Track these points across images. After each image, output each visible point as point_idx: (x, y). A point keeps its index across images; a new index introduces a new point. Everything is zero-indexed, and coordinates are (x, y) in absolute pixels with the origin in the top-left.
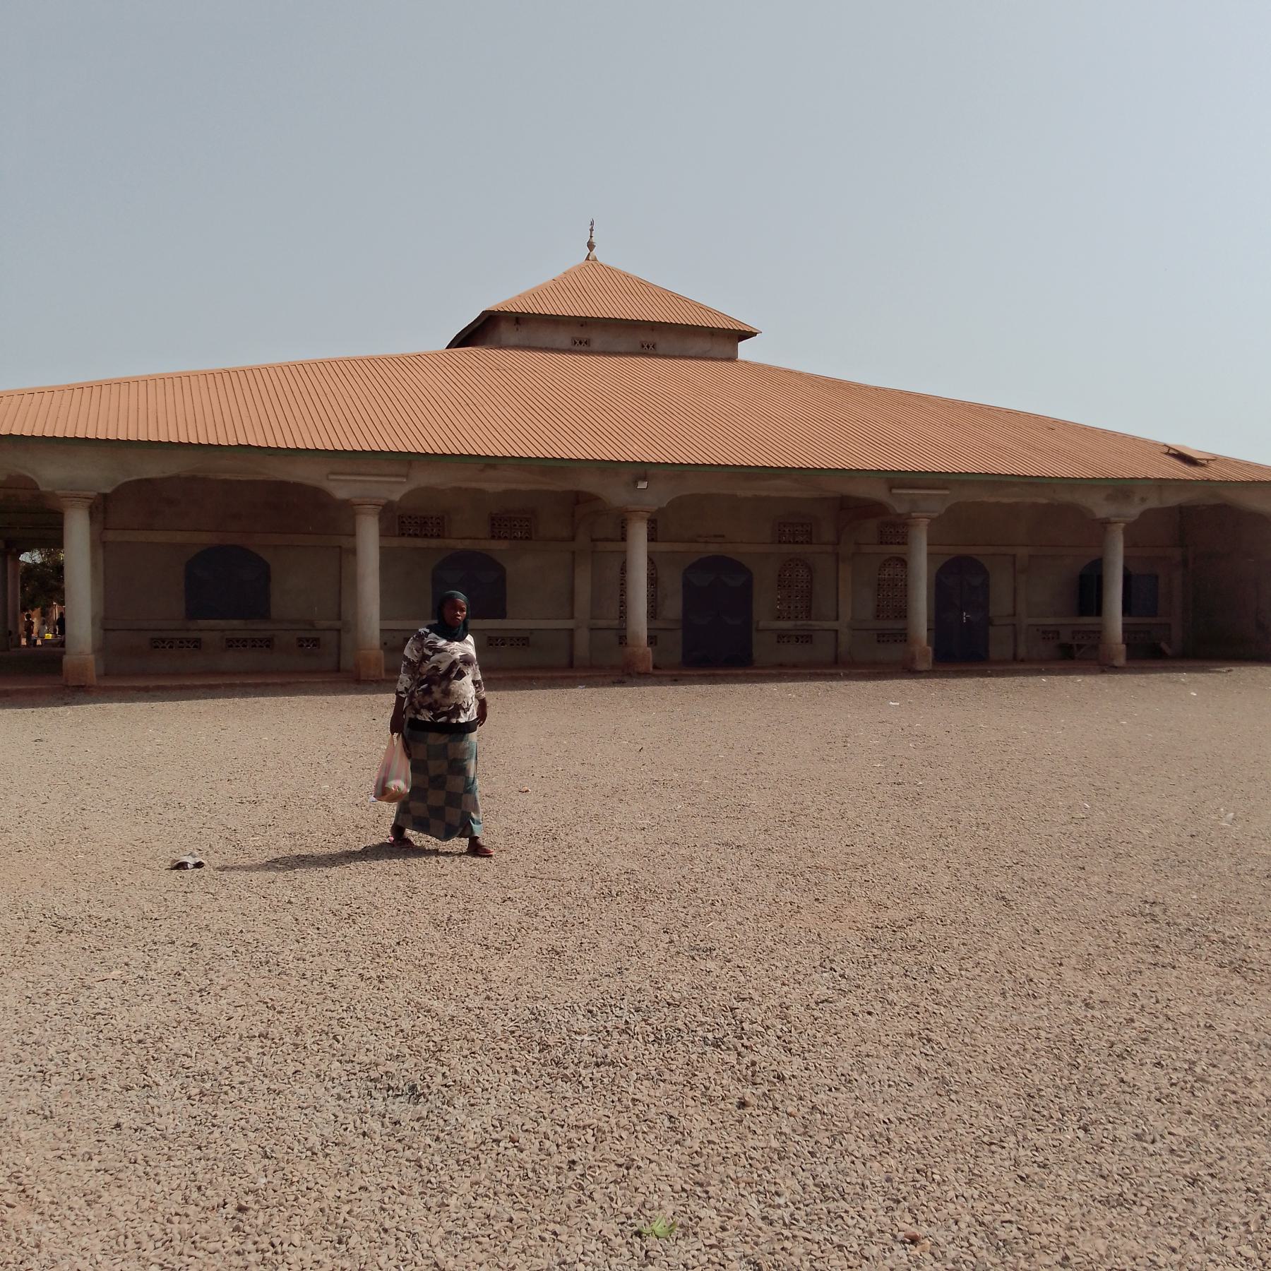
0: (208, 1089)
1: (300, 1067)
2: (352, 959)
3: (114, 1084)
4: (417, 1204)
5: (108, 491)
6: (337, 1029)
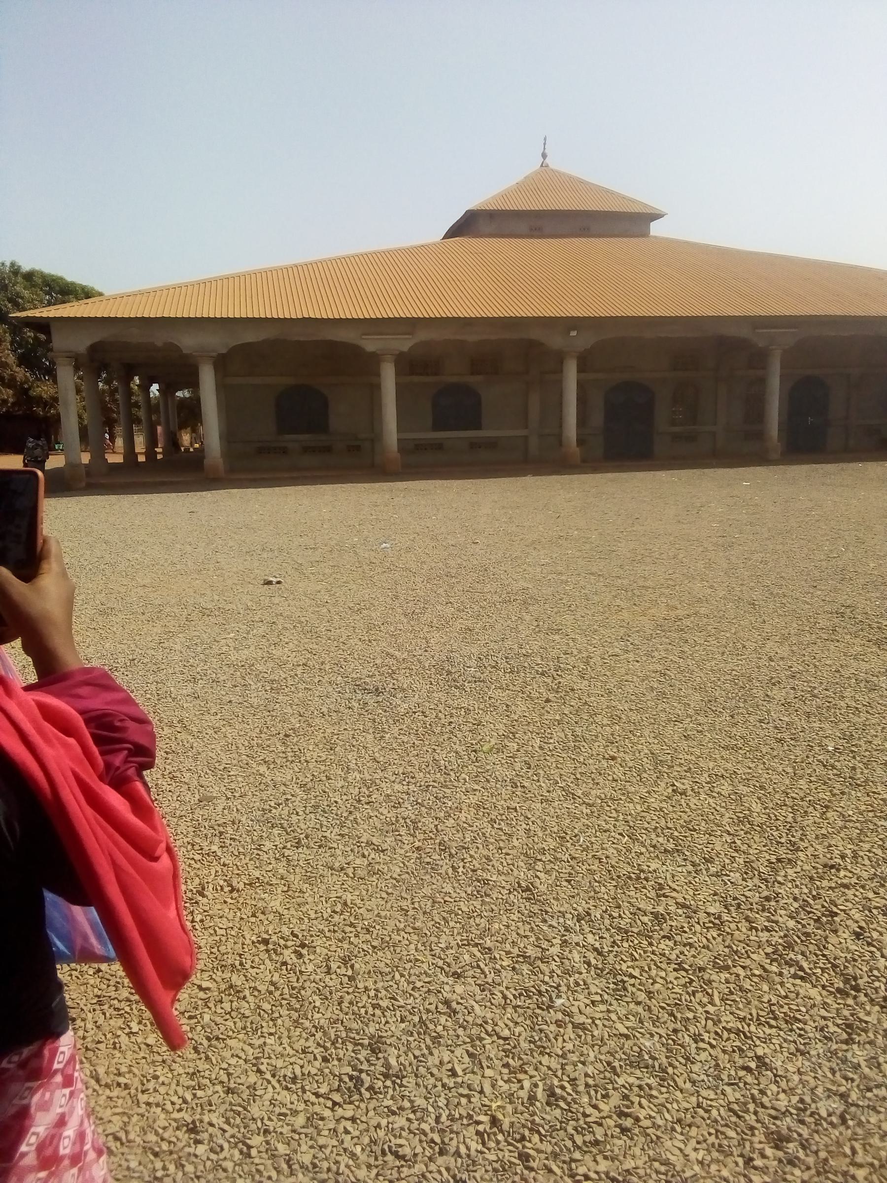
0: (276, 687)
1: (321, 678)
2: (357, 631)
3: (229, 684)
4: (370, 737)
5: (224, 351)
6: (343, 663)
